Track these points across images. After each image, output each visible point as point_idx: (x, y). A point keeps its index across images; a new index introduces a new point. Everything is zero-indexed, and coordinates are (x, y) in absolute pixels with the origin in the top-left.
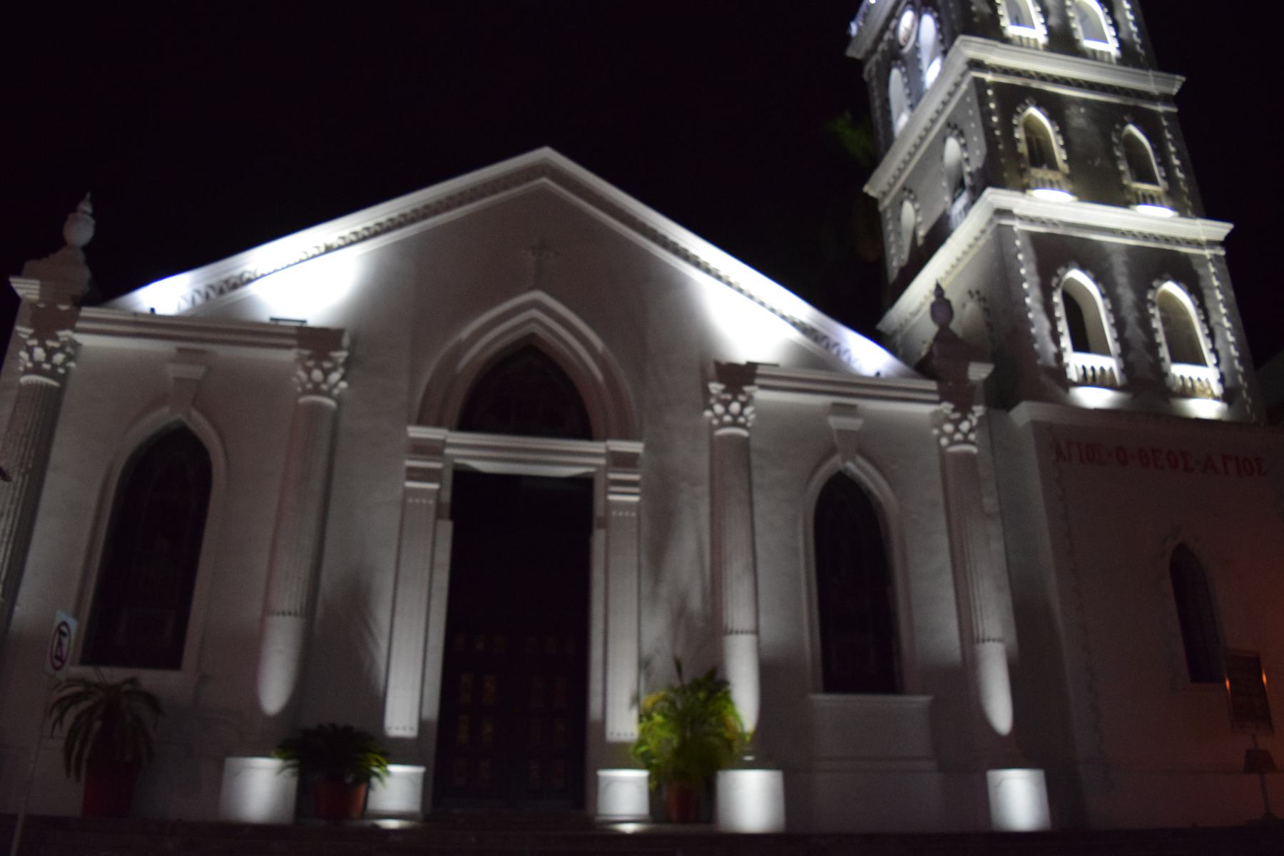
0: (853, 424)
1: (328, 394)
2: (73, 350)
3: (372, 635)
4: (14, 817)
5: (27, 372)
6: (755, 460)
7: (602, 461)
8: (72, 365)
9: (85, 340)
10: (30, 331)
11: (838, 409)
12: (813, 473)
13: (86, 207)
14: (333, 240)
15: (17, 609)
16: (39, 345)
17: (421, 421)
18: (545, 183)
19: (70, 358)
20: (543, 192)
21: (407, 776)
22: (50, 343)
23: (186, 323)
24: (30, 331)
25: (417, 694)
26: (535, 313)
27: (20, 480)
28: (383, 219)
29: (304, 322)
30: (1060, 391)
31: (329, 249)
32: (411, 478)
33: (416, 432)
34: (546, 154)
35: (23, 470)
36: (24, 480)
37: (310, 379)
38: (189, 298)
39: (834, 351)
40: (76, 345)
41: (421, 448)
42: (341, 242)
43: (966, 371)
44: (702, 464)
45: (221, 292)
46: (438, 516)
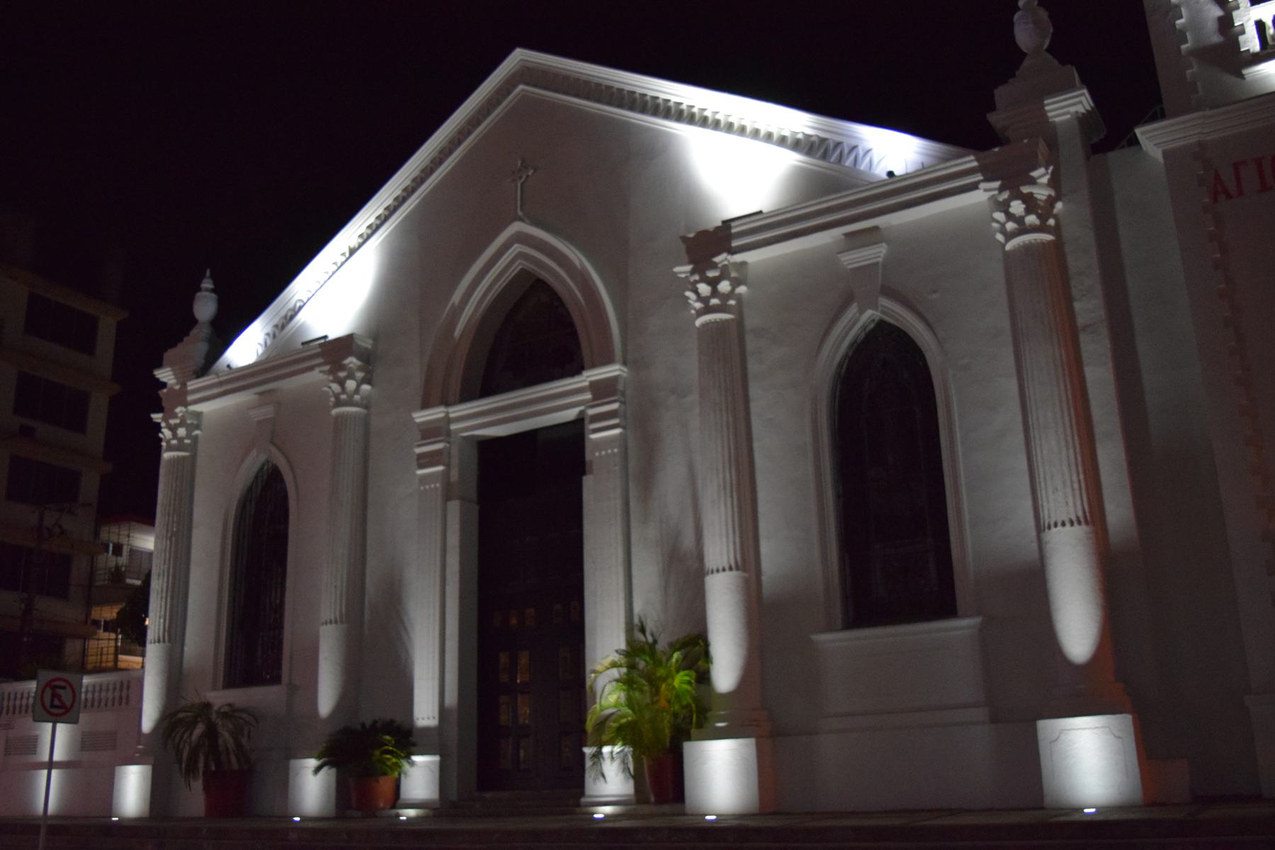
0: (877, 253)
1: (350, 403)
2: (740, 275)
3: (405, 629)
4: (39, 826)
5: (700, 313)
6: (751, 343)
7: (588, 396)
8: (742, 289)
9: (750, 257)
10: (689, 268)
11: (856, 241)
12: (827, 332)
13: (207, 284)
14: (354, 242)
15: (186, 649)
16: (701, 281)
17: (426, 405)
18: (523, 90)
19: (736, 283)
20: (525, 98)
21: (427, 765)
22: (712, 274)
23: (916, 174)
24: (689, 268)
25: (436, 683)
26: (517, 248)
27: (168, 543)
28: (389, 202)
29: (325, 337)
30: (1230, 79)
31: (352, 251)
32: (421, 466)
33: (421, 417)
34: (519, 56)
35: (169, 535)
36: (171, 542)
37: (1010, 217)
38: (262, 342)
39: (849, 162)
40: (198, 415)
41: (430, 432)
42: (361, 240)
43: (1043, 114)
44: (690, 366)
45: (283, 327)
46: (447, 498)
